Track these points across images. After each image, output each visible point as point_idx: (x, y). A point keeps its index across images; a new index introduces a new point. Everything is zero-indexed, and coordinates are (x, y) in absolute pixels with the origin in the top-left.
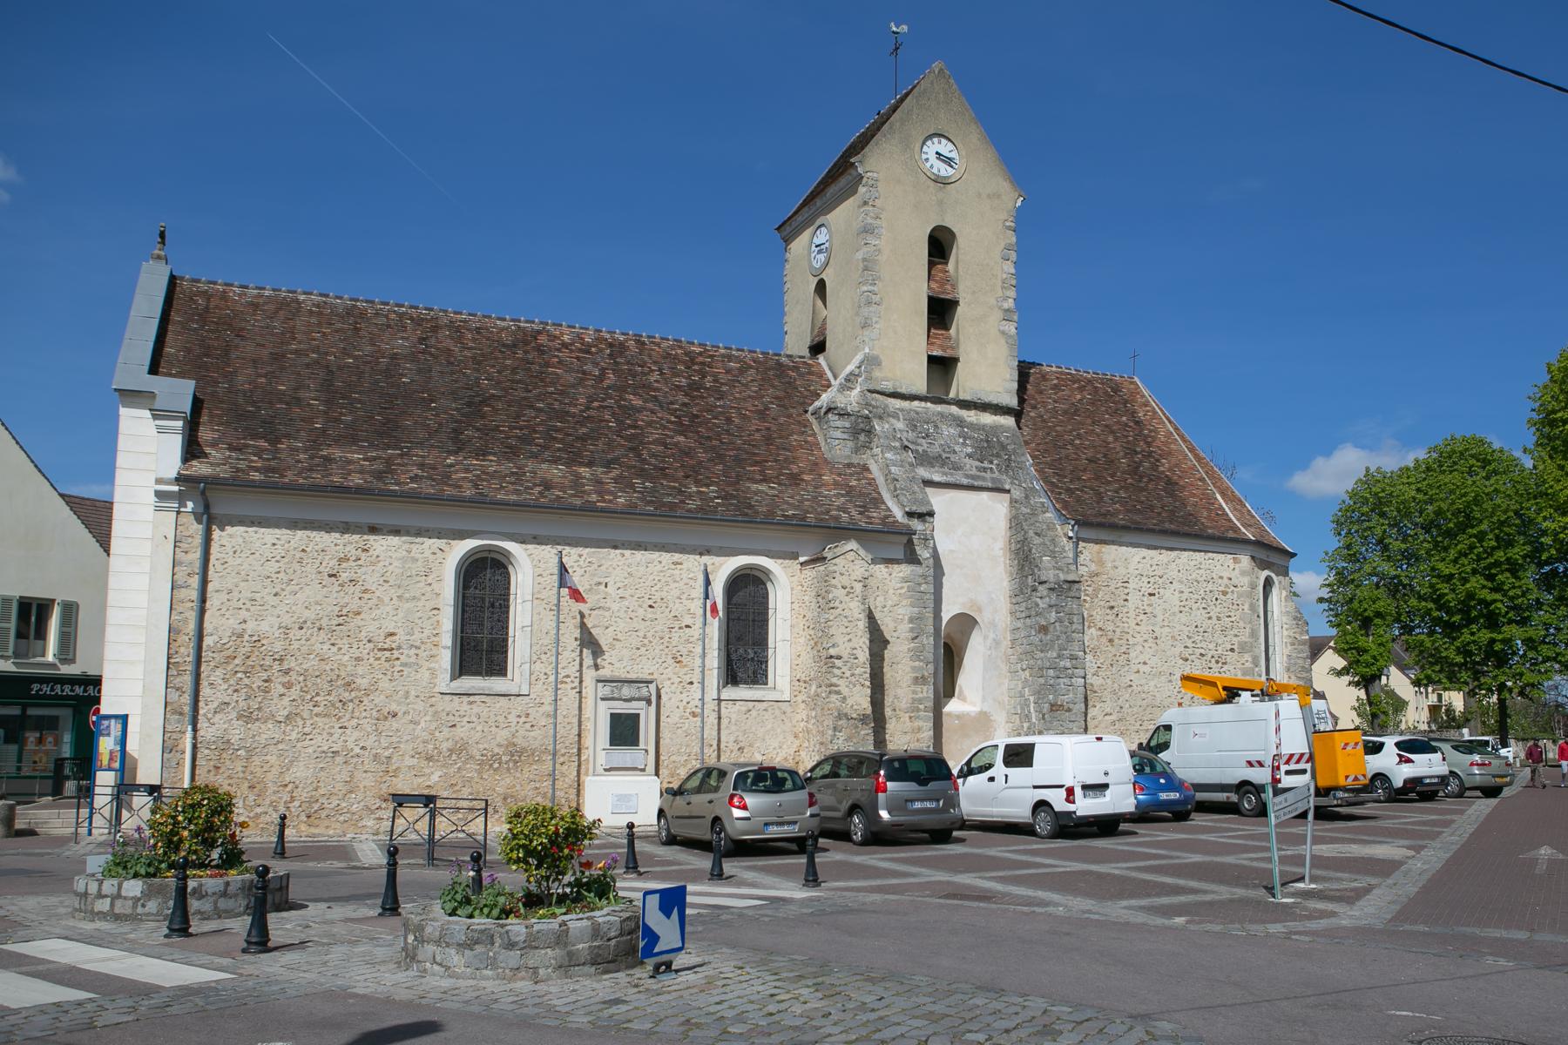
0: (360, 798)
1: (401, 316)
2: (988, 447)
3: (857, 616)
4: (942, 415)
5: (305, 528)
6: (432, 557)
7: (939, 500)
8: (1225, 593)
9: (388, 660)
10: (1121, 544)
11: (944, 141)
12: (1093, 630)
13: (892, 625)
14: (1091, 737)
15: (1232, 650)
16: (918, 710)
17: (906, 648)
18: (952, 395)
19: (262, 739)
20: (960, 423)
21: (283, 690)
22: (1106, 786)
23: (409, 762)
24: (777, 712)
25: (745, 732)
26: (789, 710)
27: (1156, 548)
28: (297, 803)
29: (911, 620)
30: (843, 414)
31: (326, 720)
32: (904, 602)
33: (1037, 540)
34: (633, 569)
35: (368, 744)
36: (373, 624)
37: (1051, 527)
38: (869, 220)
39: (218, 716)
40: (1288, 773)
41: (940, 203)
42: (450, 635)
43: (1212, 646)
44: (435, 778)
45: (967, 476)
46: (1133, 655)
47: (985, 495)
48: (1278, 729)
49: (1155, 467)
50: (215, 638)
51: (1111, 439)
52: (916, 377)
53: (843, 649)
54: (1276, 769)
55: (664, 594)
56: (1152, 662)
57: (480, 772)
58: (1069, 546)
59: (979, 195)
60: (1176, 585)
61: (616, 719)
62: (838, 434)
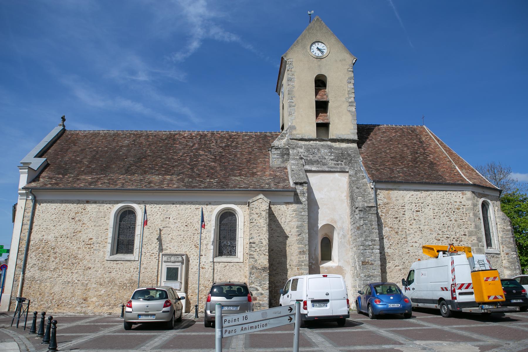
0: (76, 299)
1: (131, 134)
2: (342, 156)
3: (263, 225)
4: (323, 145)
5: (65, 203)
6: (107, 211)
7: (313, 179)
8: (458, 209)
9: (89, 248)
10: (400, 190)
11: (320, 44)
12: (387, 228)
13: (289, 230)
14: (321, 275)
16: (301, 265)
17: (295, 239)
18: (331, 136)
19: (45, 277)
20: (331, 147)
21: (53, 259)
22: (327, 301)
23: (94, 286)
24: (238, 267)
25: (223, 275)
26: (243, 266)
27: (418, 190)
28: (54, 301)
29: (297, 227)
30: (277, 148)
31: (67, 270)
32: (294, 220)
33: (357, 190)
34: (180, 212)
35: (80, 279)
36: (84, 236)
37: (365, 185)
38: (290, 76)
39: (32, 269)
40: (460, 294)
41: (319, 66)
42: (111, 238)
44: (103, 292)
45: (329, 167)
46: (409, 239)
47: (337, 175)
48: (453, 270)
49: (425, 158)
50: (34, 241)
51: (405, 149)
52: (311, 131)
53: (256, 240)
54: (453, 291)
55: (191, 221)
57: (119, 290)
58: (372, 192)
59: (336, 61)
60: (431, 206)
61: (169, 270)
62: (275, 156)
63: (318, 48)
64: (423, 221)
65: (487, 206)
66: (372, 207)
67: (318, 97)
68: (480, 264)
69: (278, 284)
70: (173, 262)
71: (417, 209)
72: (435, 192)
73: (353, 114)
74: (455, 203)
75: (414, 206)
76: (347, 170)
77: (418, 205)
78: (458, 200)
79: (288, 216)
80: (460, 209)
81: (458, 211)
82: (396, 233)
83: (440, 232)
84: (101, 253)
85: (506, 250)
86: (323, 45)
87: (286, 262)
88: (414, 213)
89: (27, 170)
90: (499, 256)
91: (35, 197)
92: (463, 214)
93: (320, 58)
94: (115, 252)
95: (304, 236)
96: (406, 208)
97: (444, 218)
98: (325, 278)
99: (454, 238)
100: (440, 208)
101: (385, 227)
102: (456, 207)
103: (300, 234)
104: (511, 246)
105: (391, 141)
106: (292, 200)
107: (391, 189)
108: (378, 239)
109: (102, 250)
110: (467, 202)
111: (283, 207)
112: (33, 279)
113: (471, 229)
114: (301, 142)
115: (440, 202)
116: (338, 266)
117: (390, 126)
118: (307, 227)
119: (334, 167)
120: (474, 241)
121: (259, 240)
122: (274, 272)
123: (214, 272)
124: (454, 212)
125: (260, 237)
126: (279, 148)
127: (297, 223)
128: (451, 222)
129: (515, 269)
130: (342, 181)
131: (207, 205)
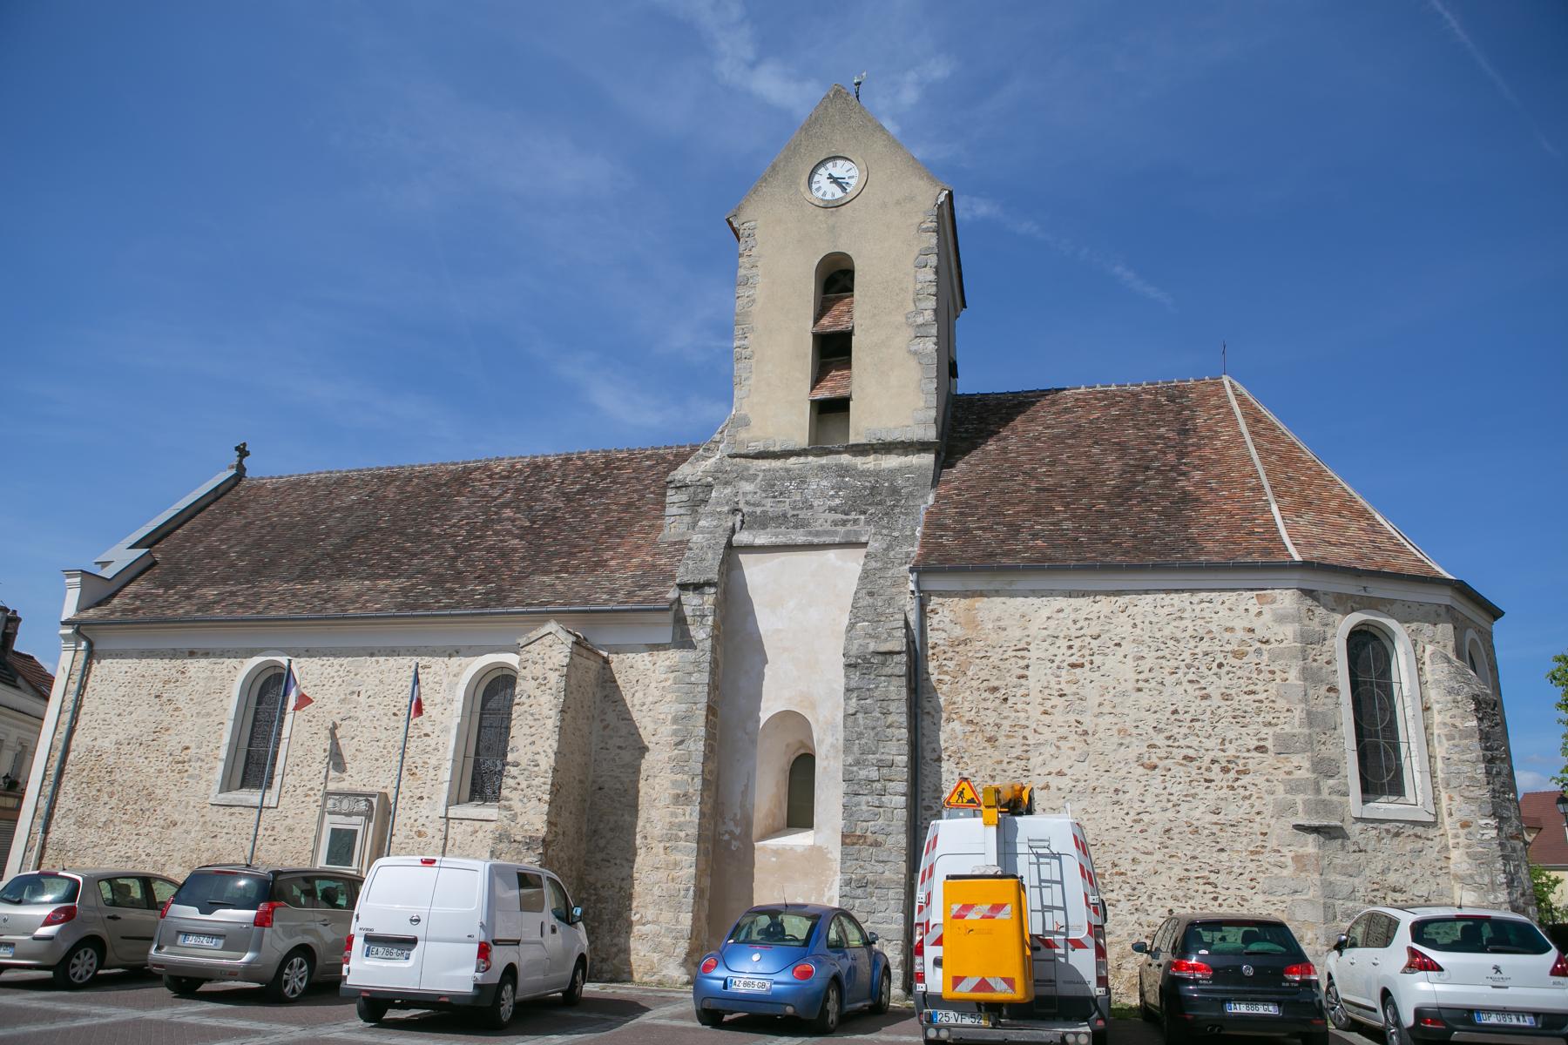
3: (546, 712)
4: (822, 467)
8: (1239, 655)
10: (1013, 594)
11: (840, 163)
12: (956, 725)
15: (1261, 749)
16: (677, 839)
17: (666, 756)
19: (85, 843)
22: (413, 942)
27: (1084, 594)
29: (675, 720)
35: (152, 851)
36: (172, 742)
43: (1212, 743)
45: (810, 533)
46: (1035, 760)
47: (831, 555)
52: (794, 426)
56: (1080, 770)
60: (1127, 647)
63: (831, 177)
64: (1094, 700)
65: (1387, 643)
66: (891, 653)
67: (825, 321)
68: (1038, 855)
69: (604, 893)
70: (347, 815)
71: (1073, 660)
72: (1149, 598)
73: (925, 361)
74: (1227, 635)
75: (1064, 649)
76: (863, 539)
77: (1077, 643)
78: (1239, 624)
79: (653, 685)
80: (1245, 654)
81: (1236, 662)
82: (989, 740)
83: (1160, 740)
84: (203, 784)
85: (1462, 810)
86: (848, 165)
87: (634, 825)
88: (1064, 673)
89: (78, 580)
90: (1431, 833)
91: (90, 644)
92: (1260, 672)
93: (833, 206)
94: (238, 784)
95: (692, 748)
96: (1034, 654)
97: (1180, 690)
98: (428, 869)
99: (1213, 762)
100: (1166, 653)
101: (948, 720)
102: (1228, 648)
103: (682, 742)
104: (1477, 793)
105: (1073, 436)
106: (666, 636)
107: (981, 594)
108: (902, 760)
109: (205, 776)
110: (1276, 628)
111: (642, 660)
112: (61, 847)
113: (1287, 728)
114: (760, 462)
115: (1167, 631)
116: (812, 848)
117: (1098, 388)
118: (701, 721)
119: (826, 533)
120: (1298, 774)
121: (530, 755)
122: (599, 856)
123: (445, 845)
124: (1220, 666)
125: (533, 748)
126: (687, 486)
127: (676, 706)
128: (1205, 703)
129: (1493, 886)
130: (842, 571)
131: (450, 656)
